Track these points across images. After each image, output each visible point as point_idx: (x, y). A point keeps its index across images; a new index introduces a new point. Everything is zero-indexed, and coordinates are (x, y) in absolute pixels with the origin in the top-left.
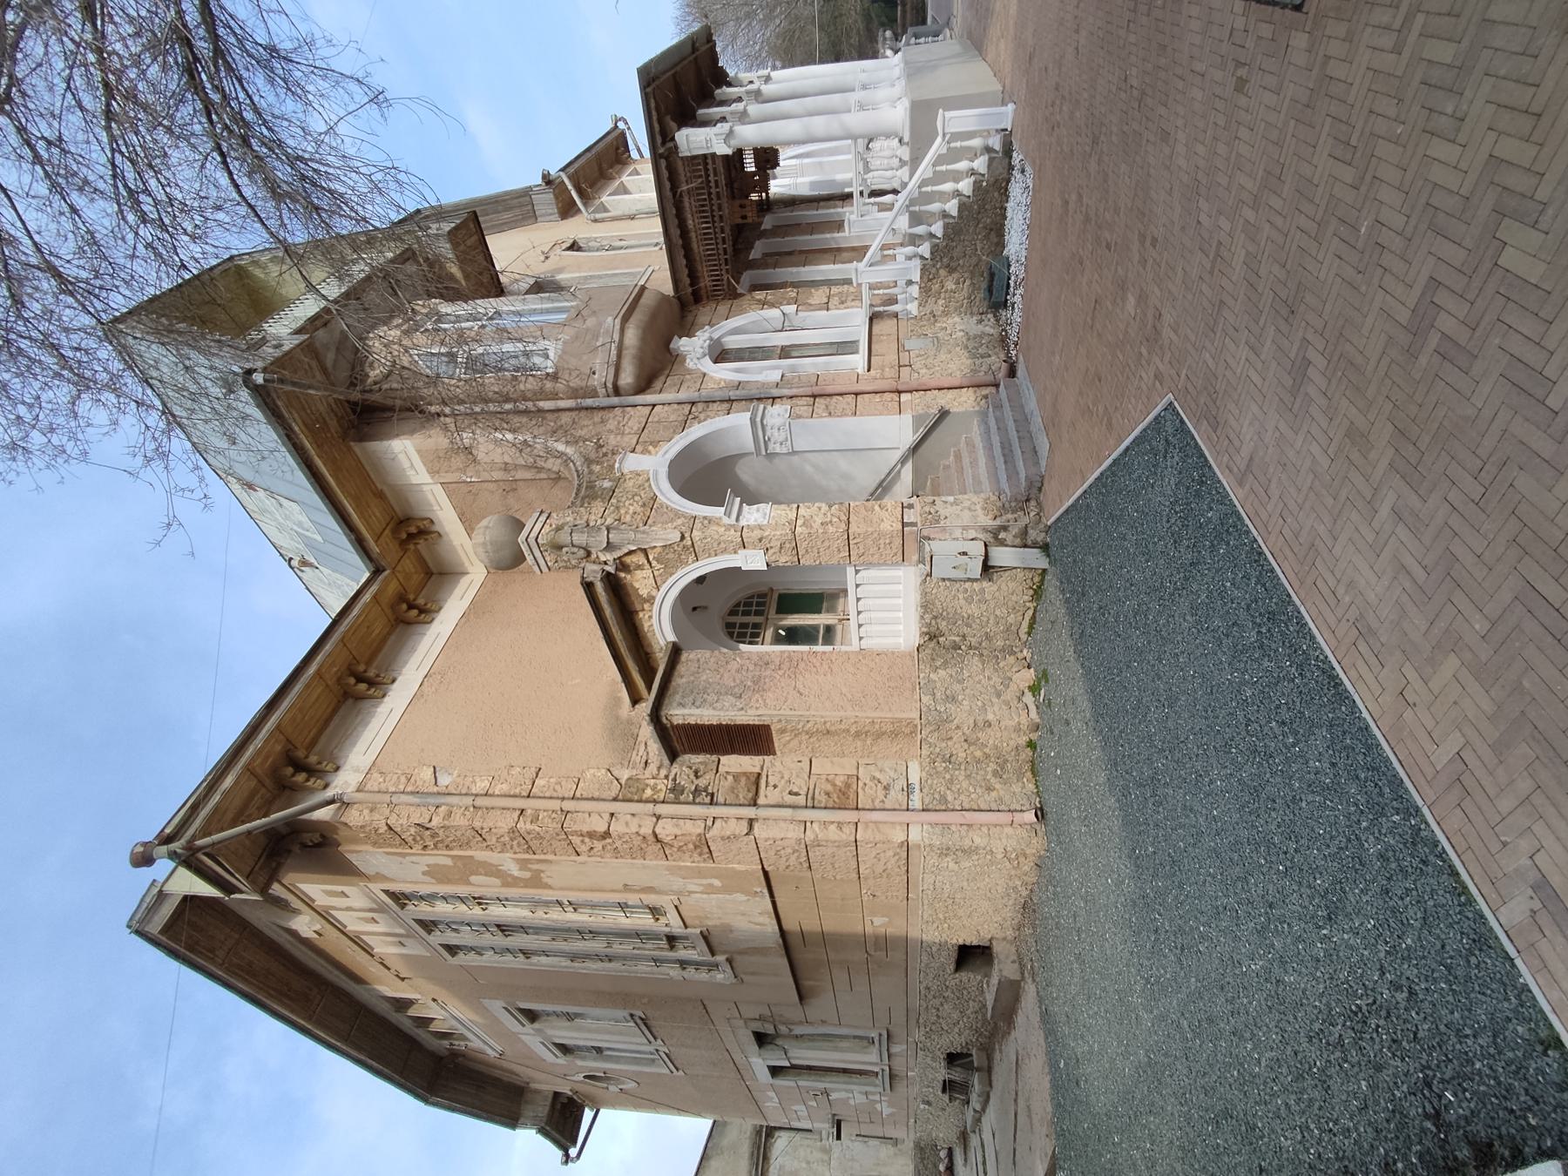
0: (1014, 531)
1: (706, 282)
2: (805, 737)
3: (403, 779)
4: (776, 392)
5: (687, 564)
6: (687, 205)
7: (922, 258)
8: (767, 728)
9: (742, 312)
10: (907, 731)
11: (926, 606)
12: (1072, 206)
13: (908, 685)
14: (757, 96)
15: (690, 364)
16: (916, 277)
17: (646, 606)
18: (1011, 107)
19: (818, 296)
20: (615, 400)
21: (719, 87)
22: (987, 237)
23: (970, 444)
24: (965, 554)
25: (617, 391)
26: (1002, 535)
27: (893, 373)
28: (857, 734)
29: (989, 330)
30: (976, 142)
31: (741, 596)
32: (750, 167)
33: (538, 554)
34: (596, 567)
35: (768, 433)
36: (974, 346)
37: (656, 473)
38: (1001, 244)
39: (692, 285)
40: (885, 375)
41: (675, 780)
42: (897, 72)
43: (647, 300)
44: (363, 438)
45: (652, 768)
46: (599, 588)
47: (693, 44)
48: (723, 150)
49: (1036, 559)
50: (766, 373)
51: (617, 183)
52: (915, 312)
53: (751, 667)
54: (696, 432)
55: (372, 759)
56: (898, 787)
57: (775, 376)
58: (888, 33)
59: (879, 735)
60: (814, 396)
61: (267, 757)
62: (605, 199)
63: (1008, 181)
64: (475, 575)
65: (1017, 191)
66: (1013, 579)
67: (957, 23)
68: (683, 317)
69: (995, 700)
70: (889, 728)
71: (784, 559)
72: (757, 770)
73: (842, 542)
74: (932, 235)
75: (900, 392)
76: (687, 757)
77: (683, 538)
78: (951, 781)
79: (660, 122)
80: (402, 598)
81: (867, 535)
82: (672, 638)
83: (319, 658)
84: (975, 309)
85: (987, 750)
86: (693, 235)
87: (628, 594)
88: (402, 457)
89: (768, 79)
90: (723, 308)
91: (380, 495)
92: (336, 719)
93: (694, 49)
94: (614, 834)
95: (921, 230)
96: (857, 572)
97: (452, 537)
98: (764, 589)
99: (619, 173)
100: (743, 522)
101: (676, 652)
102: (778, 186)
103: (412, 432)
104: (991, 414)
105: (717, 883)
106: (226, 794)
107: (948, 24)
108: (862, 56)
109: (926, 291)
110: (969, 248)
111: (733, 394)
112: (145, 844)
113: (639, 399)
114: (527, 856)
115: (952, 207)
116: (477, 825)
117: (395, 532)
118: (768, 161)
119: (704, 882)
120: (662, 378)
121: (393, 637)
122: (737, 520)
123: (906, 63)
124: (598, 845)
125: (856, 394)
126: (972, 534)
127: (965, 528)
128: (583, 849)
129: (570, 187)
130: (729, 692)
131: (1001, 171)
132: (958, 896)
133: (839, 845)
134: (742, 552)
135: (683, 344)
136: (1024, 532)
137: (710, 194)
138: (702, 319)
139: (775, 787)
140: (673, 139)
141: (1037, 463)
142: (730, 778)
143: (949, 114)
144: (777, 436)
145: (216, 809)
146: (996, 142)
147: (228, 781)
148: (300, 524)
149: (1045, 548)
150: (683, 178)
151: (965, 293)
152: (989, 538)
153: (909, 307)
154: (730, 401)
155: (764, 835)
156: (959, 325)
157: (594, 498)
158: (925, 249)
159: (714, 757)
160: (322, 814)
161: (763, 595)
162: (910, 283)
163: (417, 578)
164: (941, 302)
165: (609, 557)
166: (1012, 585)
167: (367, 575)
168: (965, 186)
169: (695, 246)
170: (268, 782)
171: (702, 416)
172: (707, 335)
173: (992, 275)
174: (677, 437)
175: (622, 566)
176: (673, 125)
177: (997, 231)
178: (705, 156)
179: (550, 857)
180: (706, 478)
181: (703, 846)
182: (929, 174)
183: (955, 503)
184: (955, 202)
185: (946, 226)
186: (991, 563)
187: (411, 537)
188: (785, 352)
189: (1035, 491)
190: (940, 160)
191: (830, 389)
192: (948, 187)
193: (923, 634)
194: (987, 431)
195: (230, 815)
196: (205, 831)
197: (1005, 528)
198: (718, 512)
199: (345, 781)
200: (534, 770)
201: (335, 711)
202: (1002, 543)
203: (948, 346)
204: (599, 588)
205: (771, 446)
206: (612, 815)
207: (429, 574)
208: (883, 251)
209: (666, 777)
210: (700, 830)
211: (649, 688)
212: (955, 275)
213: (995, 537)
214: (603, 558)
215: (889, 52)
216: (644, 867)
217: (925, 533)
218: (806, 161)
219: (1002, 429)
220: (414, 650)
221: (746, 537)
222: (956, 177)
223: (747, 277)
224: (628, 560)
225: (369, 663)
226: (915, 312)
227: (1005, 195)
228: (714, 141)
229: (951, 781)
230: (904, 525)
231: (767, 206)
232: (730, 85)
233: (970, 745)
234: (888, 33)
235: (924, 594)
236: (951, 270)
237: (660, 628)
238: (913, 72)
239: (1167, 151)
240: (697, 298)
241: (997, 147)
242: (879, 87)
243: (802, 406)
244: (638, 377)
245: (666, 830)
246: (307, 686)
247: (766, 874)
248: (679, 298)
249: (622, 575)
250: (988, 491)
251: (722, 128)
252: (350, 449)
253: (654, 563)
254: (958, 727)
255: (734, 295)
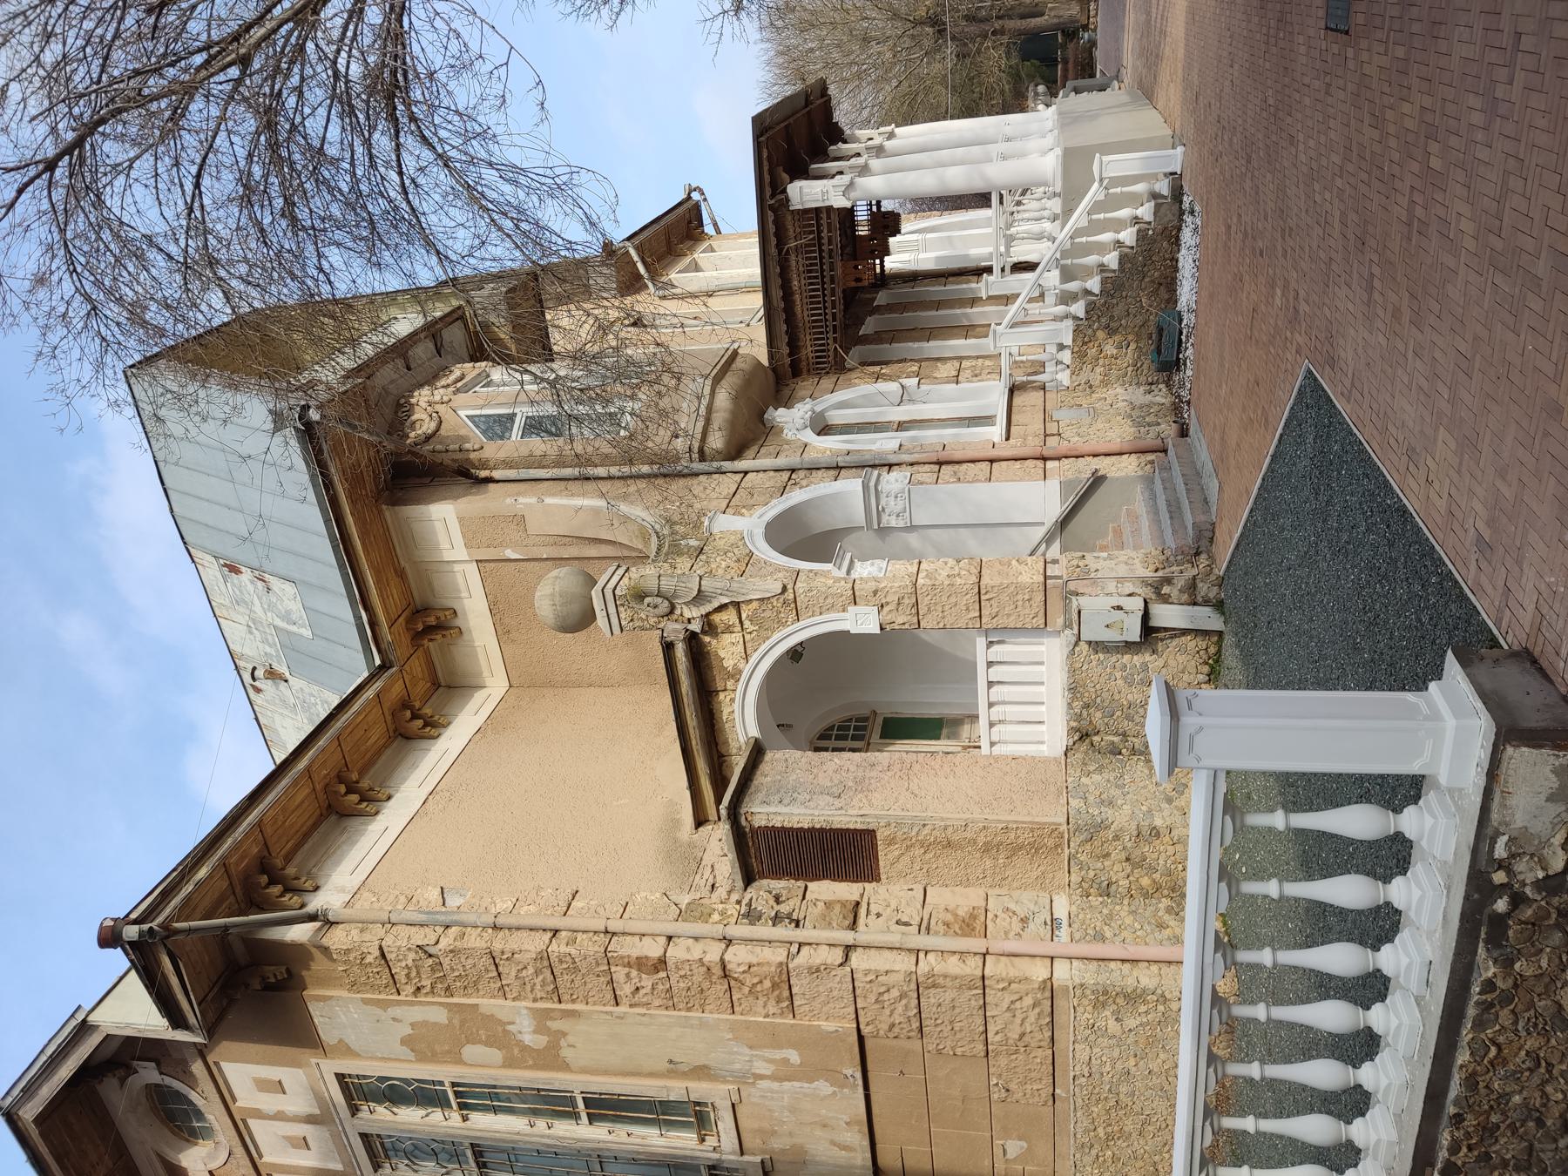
0: (1180, 583)
1: (808, 351)
2: (918, 851)
3: (403, 899)
4: (893, 459)
5: (785, 624)
6: (793, 263)
7: (1076, 318)
8: (871, 833)
9: (850, 385)
10: (1050, 843)
11: (1074, 689)
12: (1234, 228)
13: (1053, 789)
14: (879, 151)
15: (789, 434)
16: (1068, 341)
17: (730, 684)
18: (1180, 149)
19: (947, 370)
20: (697, 466)
21: (835, 143)
22: (1155, 292)
23: (1134, 517)
24: (1119, 608)
25: (702, 457)
26: (1166, 590)
27: (1039, 441)
28: (987, 848)
29: (1159, 399)
30: (1140, 187)
31: (834, 719)
32: (863, 231)
33: (612, 610)
34: (678, 626)
35: (883, 502)
36: (1140, 416)
37: (751, 535)
38: (1173, 300)
39: (790, 355)
40: (1028, 435)
41: (749, 904)
42: (1050, 124)
43: (738, 364)
44: (395, 502)
45: (721, 892)
46: (680, 651)
47: (807, 96)
48: (840, 202)
49: (1207, 618)
50: (884, 444)
51: (687, 260)
52: (1066, 382)
53: (852, 768)
54: (796, 497)
55: (359, 880)
56: (1040, 919)
57: (894, 445)
58: (1041, 88)
59: (1015, 849)
60: (940, 463)
61: (242, 858)
62: (673, 276)
63: (1179, 229)
64: (495, 686)
65: (1187, 236)
66: (1183, 650)
67: (1128, 76)
68: (777, 391)
69: (1165, 805)
70: (1025, 838)
71: (902, 619)
72: (856, 897)
73: (971, 598)
74: (1087, 292)
75: (1045, 459)
76: (765, 882)
77: (784, 589)
78: (1110, 916)
79: (771, 172)
80: (405, 704)
81: (1002, 588)
82: (754, 732)
83: (270, 798)
84: (1143, 379)
85: (1157, 876)
86: (797, 297)
87: (710, 667)
88: (439, 526)
89: (891, 136)
90: (827, 382)
91: (401, 574)
92: (316, 836)
93: (807, 102)
94: (670, 963)
95: (1074, 286)
96: (990, 644)
97: (475, 634)
98: (865, 712)
99: (692, 249)
100: (855, 575)
101: (757, 753)
102: (892, 263)
103: (456, 498)
104: (1158, 482)
105: (794, 1056)
106: (199, 885)
107: (1117, 77)
108: (1006, 110)
109: (1080, 355)
110: (1135, 306)
111: (841, 461)
112: (115, 920)
113: (727, 465)
114: (549, 1005)
115: (1112, 259)
116: (497, 946)
117: (410, 621)
118: (886, 227)
119: (778, 1055)
120: (756, 448)
121: (389, 752)
122: (848, 572)
123: (1060, 114)
124: (647, 981)
125: (992, 461)
126: (1129, 588)
127: (1120, 580)
128: (625, 990)
129: (636, 258)
130: (826, 792)
131: (1169, 217)
132: (1123, 1089)
133: (963, 984)
134: (851, 609)
135: (780, 415)
136: (1192, 586)
137: (821, 251)
138: (801, 393)
139: (878, 915)
140: (784, 191)
141: (1207, 511)
142: (820, 905)
143: (1106, 159)
144: (892, 505)
145: (188, 898)
146: (1163, 187)
147: (202, 873)
148: (287, 617)
149: (1219, 606)
150: (791, 233)
151: (1129, 359)
152: (1148, 592)
153: (1059, 376)
154: (838, 468)
155: (865, 966)
156: (1123, 395)
157: (680, 554)
158: (1079, 308)
159: (801, 883)
160: (298, 933)
161: (866, 719)
162: (1061, 347)
163: (422, 686)
164: (1099, 370)
165: (695, 612)
166: (1181, 659)
167: (366, 674)
168: (1128, 236)
169: (798, 309)
170: (238, 890)
171: (804, 483)
172: (808, 407)
173: (1160, 331)
174: (774, 501)
175: (710, 627)
176: (786, 176)
177: (1168, 284)
178: (817, 210)
179: (578, 1007)
180: (805, 539)
181: (783, 981)
182: (1084, 223)
183: (1110, 558)
184: (1115, 254)
185: (1104, 282)
186: (1154, 623)
187: (429, 630)
188: (901, 426)
189: (1204, 543)
190: (1097, 207)
191: (958, 456)
192: (1107, 237)
193: (1072, 730)
194: (1153, 497)
195: (206, 903)
196: (185, 911)
197: (1168, 581)
198: (829, 566)
199: (327, 899)
200: (569, 892)
201: (315, 826)
202: (1166, 599)
203: (1107, 414)
204: (680, 651)
205: (885, 518)
206: (670, 938)
207: (436, 685)
208: (1029, 328)
209: (739, 902)
210: (783, 958)
211: (718, 801)
212: (1117, 338)
213: (1158, 589)
214: (687, 614)
215: (1041, 107)
216: (703, 1025)
217: (1072, 586)
218: (929, 236)
219: (1169, 486)
220: (415, 766)
221: (850, 601)
222: (1118, 225)
223: (856, 351)
224: (716, 618)
225: (363, 772)
226: (1066, 382)
227: (1177, 242)
228: (832, 193)
229: (1110, 916)
230: (1045, 578)
231: (884, 280)
232: (845, 142)
233: (1136, 865)
234: (1041, 88)
235: (1072, 671)
236: (1111, 332)
237: (742, 718)
238: (1067, 122)
239: (1293, 151)
240: (796, 371)
241: (1165, 192)
242: (1026, 142)
243: (925, 474)
244: (728, 443)
245: (738, 957)
246: (295, 783)
247: (861, 1039)
248: (774, 370)
249: (707, 639)
250: (1150, 547)
251: (843, 180)
252: (380, 512)
253: (747, 624)
254: (1116, 838)
255: (840, 368)
